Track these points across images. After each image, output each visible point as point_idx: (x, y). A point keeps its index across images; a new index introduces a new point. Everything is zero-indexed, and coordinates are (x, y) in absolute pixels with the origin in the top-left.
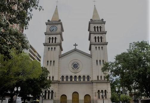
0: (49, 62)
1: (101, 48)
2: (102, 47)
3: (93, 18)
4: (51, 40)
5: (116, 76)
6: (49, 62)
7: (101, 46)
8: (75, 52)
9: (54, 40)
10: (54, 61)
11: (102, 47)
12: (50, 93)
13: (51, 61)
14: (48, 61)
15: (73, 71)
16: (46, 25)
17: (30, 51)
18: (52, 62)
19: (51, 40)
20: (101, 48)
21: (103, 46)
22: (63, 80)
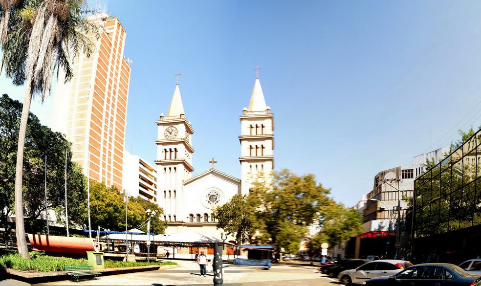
0: (167, 193)
1: (173, 169)
2: (175, 168)
3: (157, 129)
4: (168, 154)
5: (90, 192)
6: (167, 193)
7: (172, 167)
8: (211, 174)
9: (173, 154)
10: (175, 191)
11: (175, 168)
12: (312, 263)
13: (170, 191)
14: (165, 192)
15: (208, 205)
16: (20, 129)
17: (140, 170)
18: (172, 193)
19: (168, 154)
20: (173, 169)
21: (175, 166)
22: (192, 220)
